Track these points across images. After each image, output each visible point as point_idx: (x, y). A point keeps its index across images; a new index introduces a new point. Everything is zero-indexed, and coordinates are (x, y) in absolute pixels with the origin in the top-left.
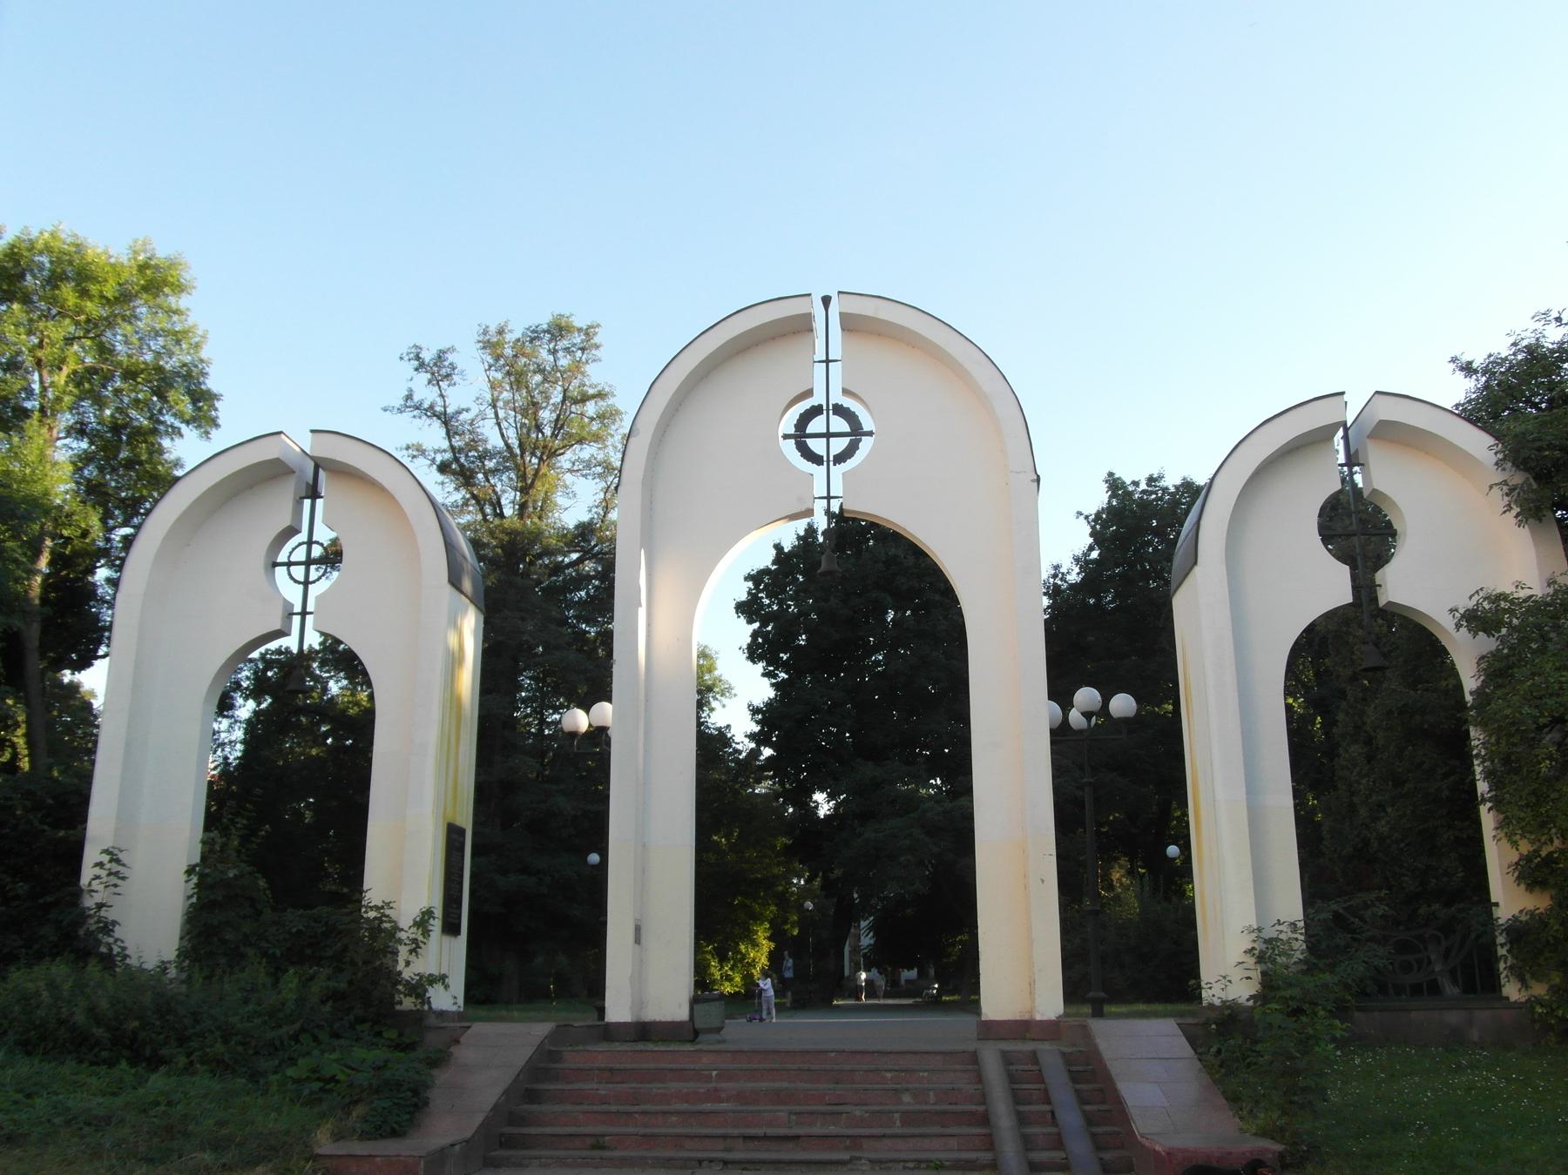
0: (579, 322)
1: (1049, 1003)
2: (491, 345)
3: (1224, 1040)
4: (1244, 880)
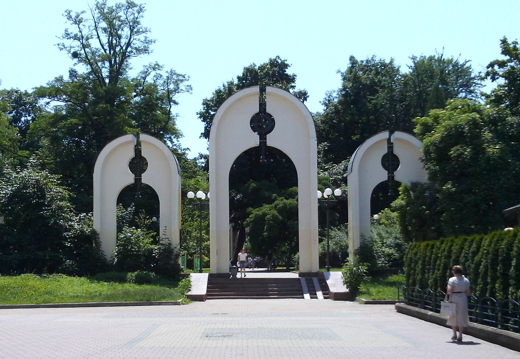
2: (100, 8)
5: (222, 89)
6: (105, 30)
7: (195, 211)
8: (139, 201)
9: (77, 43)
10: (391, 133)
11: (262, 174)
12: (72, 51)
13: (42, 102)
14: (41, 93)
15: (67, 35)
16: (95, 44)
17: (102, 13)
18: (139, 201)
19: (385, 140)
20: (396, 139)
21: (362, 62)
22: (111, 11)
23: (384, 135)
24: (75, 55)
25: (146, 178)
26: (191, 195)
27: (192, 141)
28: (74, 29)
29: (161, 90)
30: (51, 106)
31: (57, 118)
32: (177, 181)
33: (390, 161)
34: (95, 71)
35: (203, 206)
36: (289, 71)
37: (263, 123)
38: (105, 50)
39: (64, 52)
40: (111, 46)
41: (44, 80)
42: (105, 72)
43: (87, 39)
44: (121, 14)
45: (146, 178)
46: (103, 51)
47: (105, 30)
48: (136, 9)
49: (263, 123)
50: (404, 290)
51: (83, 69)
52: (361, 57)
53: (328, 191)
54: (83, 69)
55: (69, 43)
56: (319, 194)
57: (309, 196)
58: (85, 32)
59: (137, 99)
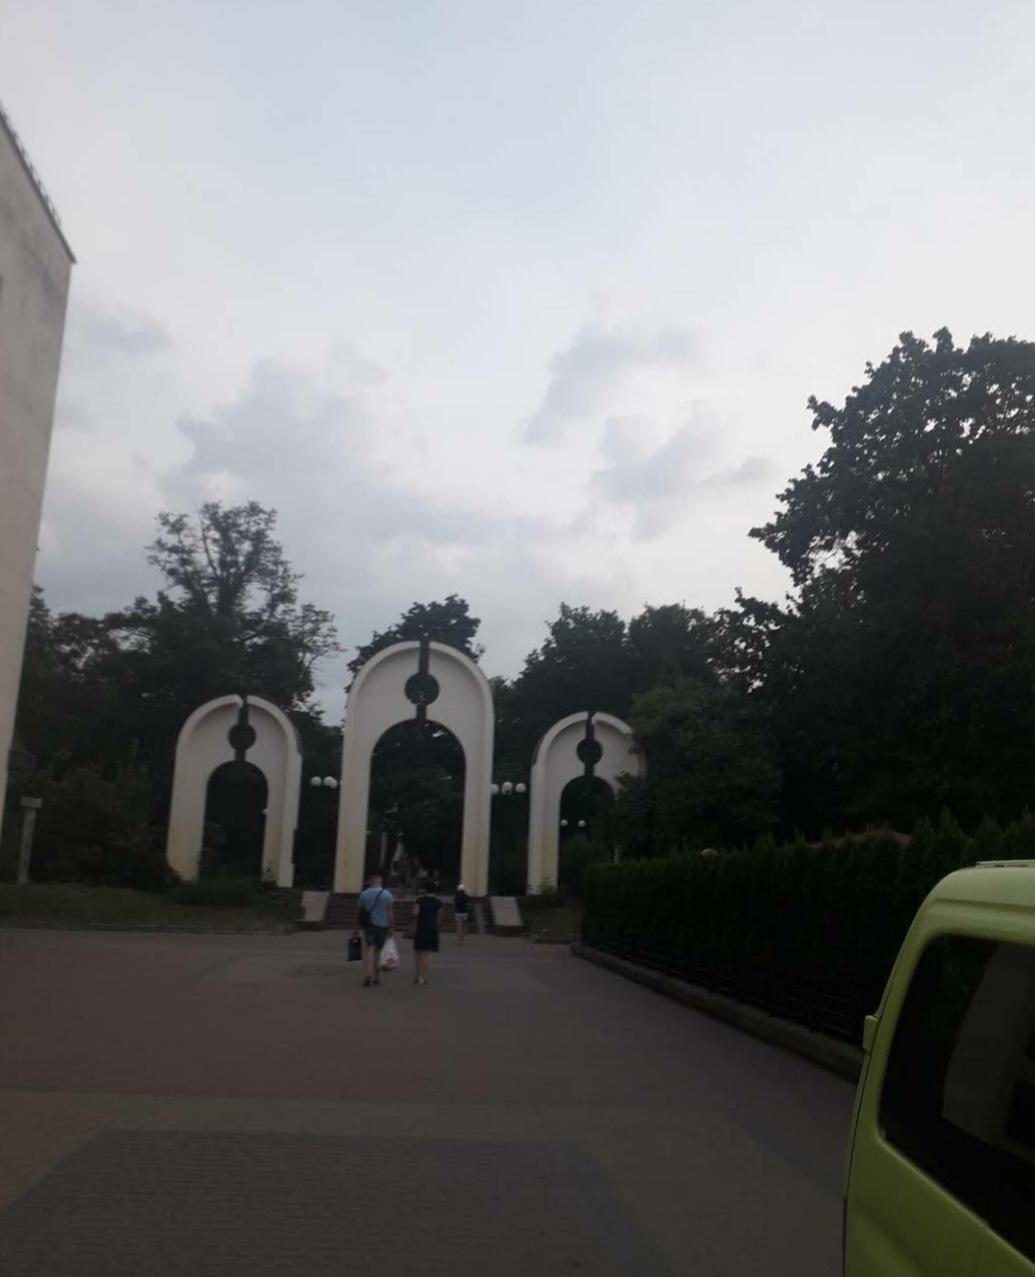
0: (265, 506)
1: (482, 891)
3: (531, 906)
4: (542, 867)
5: (763, 542)
6: (215, 541)
7: (318, 810)
8: (237, 794)
9: (175, 557)
10: (500, 792)
11: (416, 759)
12: (168, 566)
13: (118, 634)
14: (115, 621)
15: (160, 545)
16: (201, 558)
17: (214, 518)
18: (237, 794)
19: (583, 722)
20: (602, 724)
21: (577, 609)
22: (226, 516)
23: (583, 716)
24: (172, 572)
25: (252, 756)
26: (316, 780)
27: (329, 696)
28: (171, 540)
29: (292, 629)
30: (127, 641)
31: (132, 656)
32: (296, 761)
33: (589, 752)
34: (199, 599)
35: (334, 795)
36: (471, 614)
37: (422, 689)
38: (214, 569)
39: (157, 567)
40: (223, 564)
41: (123, 604)
42: (212, 599)
43: (190, 552)
44: (241, 521)
45: (252, 756)
46: (210, 570)
47: (215, 541)
48: (262, 516)
49: (422, 689)
50: (810, 573)
51: (178, 595)
52: (575, 604)
53: (508, 785)
54: (178, 595)
55: (164, 556)
56: (495, 788)
57: (479, 789)
58: (188, 542)
59: (258, 641)
